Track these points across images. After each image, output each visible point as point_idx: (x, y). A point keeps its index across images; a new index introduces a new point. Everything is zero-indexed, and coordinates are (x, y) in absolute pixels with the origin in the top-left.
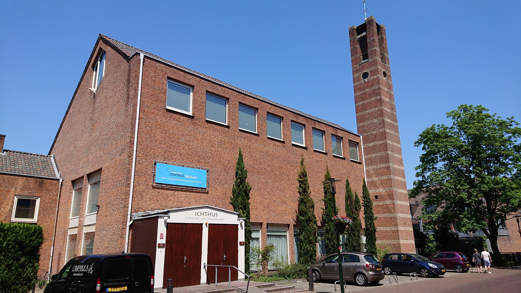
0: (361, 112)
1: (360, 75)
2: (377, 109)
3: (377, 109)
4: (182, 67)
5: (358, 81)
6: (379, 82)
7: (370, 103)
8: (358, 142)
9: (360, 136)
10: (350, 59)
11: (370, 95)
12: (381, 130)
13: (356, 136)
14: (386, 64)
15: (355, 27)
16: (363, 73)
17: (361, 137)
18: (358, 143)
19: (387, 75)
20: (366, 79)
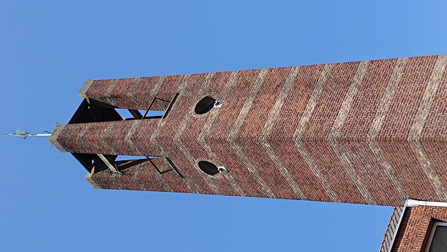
0: (323, 191)
1: (212, 179)
2: (303, 153)
3: (303, 153)
4: (386, 235)
5: (229, 185)
6: (220, 141)
7: (290, 166)
8: (427, 221)
9: (408, 209)
10: (173, 194)
11: (266, 165)
12: (377, 151)
13: (406, 233)
14: (178, 94)
15: (90, 175)
16: (203, 172)
17: (410, 203)
18: (433, 221)
19: (207, 95)
20: (219, 168)
